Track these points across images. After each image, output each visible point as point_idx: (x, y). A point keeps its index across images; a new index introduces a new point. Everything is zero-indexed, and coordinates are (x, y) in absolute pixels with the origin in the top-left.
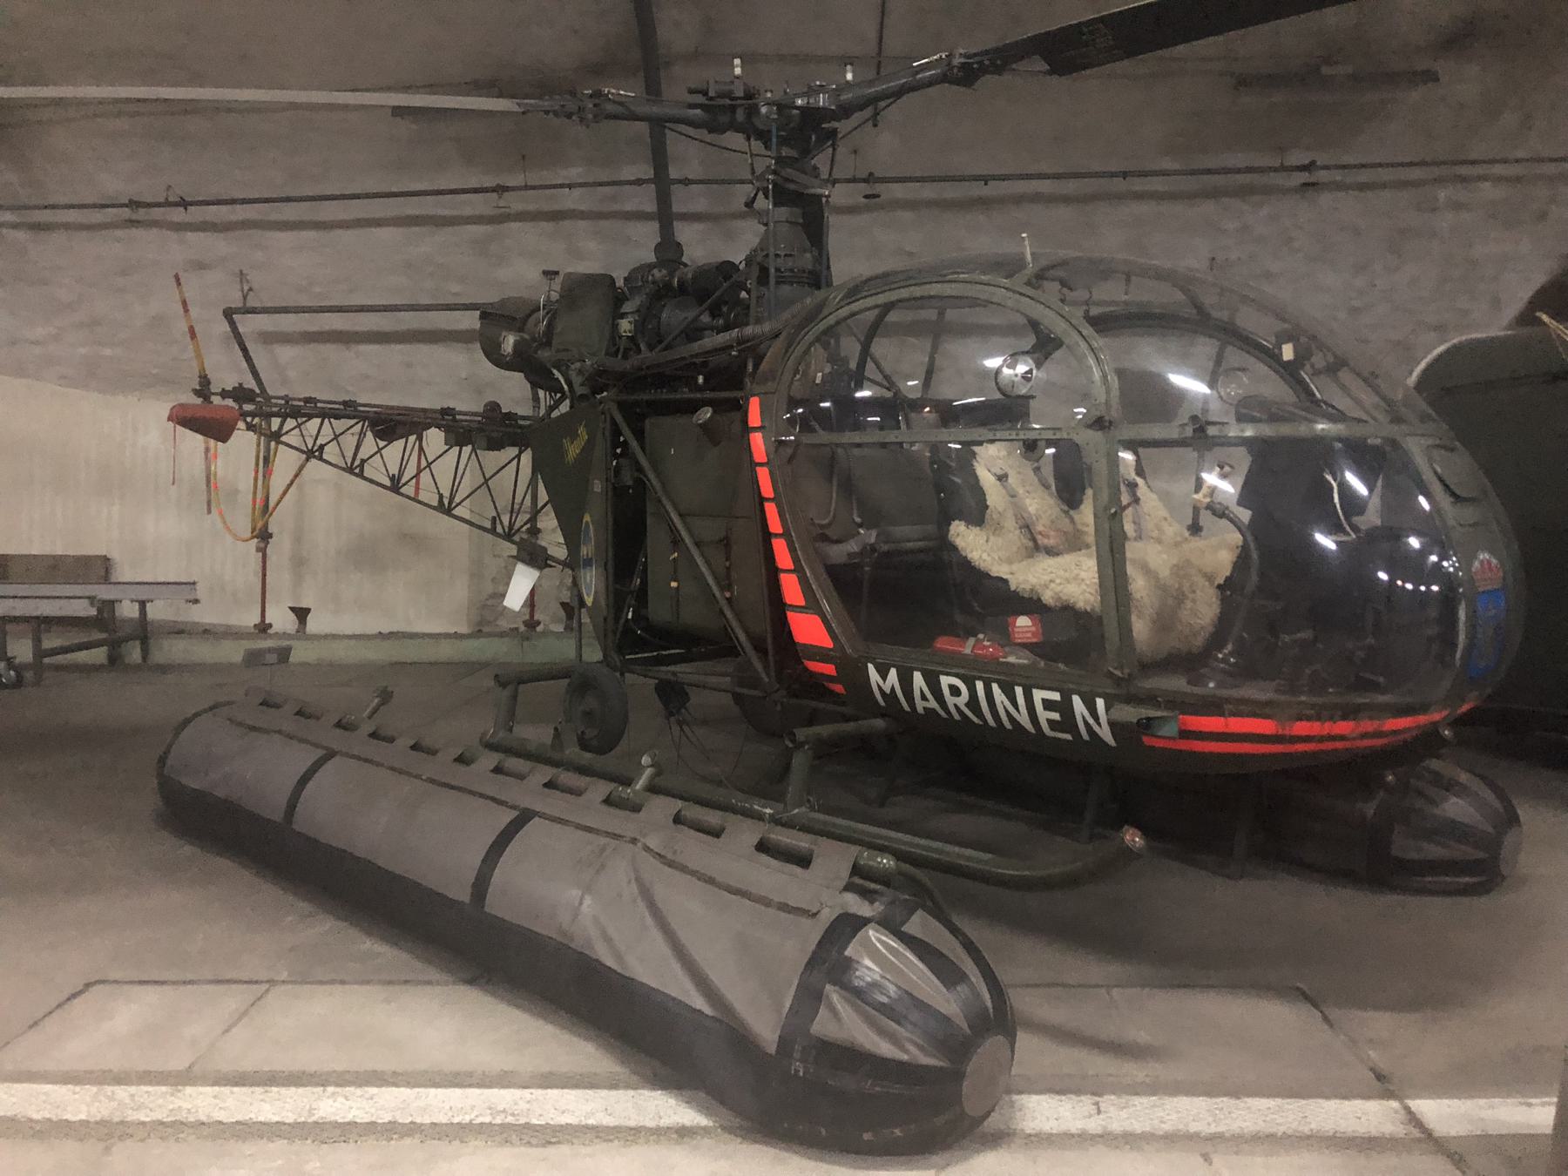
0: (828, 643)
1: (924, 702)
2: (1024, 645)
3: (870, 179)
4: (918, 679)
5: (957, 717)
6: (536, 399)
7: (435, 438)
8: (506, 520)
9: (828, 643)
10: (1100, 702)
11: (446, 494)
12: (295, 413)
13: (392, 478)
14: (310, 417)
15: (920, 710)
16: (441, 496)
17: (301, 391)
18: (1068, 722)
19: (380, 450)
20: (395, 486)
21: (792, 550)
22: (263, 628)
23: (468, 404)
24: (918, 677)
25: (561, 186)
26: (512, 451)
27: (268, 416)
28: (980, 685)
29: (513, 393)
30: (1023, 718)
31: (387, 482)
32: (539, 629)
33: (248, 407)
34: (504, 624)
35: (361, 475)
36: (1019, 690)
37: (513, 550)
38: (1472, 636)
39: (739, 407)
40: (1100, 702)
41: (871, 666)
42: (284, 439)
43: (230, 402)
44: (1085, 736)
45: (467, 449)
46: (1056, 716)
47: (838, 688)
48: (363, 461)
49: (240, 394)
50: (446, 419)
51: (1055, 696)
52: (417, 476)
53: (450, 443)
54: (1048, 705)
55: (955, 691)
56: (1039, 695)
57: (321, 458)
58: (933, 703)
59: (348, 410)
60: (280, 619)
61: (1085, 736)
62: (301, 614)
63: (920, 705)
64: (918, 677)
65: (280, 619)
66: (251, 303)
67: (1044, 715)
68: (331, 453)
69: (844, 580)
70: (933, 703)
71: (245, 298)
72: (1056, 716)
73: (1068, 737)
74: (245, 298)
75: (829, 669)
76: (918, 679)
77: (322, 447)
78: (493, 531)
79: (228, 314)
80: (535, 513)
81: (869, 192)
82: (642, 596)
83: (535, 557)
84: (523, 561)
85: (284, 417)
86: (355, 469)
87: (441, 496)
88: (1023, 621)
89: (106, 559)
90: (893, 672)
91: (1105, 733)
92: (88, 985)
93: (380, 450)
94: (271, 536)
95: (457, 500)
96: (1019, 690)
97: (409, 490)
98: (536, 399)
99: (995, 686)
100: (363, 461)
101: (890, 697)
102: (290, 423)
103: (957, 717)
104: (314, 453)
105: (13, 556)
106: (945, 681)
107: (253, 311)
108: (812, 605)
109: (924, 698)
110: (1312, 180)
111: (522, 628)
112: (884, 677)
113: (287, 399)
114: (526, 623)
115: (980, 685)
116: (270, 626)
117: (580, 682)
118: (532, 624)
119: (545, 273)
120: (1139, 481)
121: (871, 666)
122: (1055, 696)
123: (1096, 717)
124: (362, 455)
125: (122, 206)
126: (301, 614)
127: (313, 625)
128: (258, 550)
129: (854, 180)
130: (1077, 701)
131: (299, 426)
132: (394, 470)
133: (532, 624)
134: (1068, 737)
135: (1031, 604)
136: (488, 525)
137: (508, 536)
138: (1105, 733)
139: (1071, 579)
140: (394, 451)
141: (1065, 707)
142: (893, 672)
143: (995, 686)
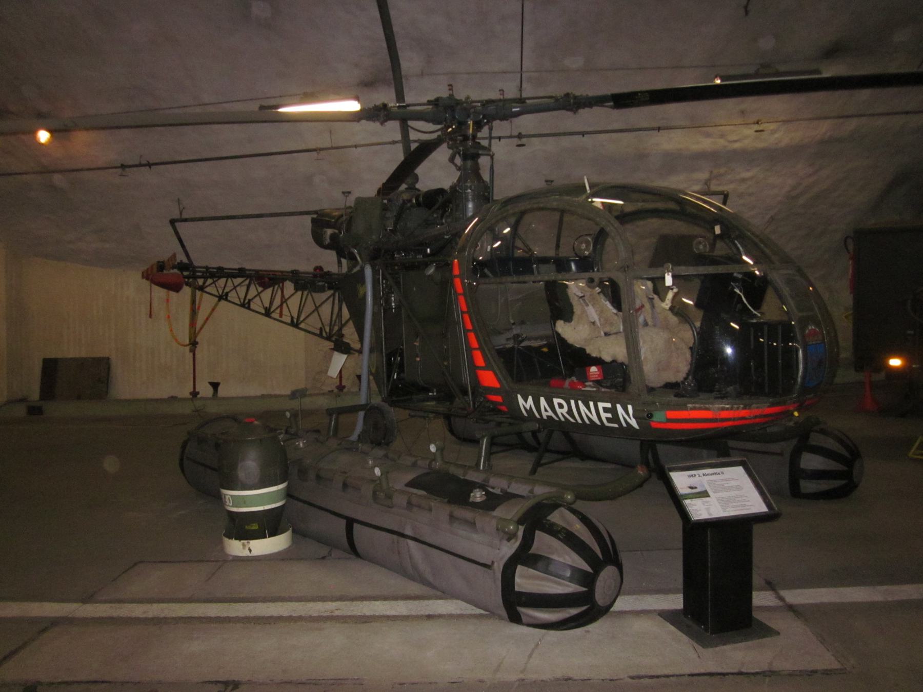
0: (498, 386)
1: (547, 413)
2: (593, 381)
3: (520, 136)
4: (543, 401)
5: (563, 419)
6: (340, 263)
7: (289, 287)
8: (327, 329)
9: (498, 386)
10: (630, 407)
11: (295, 316)
12: (212, 276)
13: (266, 309)
14: (219, 278)
15: (545, 417)
16: (292, 318)
17: (214, 264)
18: (615, 418)
19: (259, 294)
20: (268, 313)
21: (477, 337)
22: (195, 394)
23: (306, 267)
24: (542, 400)
25: (350, 147)
26: (331, 292)
27: (196, 278)
28: (572, 402)
29: (329, 261)
30: (595, 418)
31: (263, 311)
32: (345, 390)
33: (186, 273)
34: (327, 389)
35: (249, 308)
36: (591, 404)
37: (332, 345)
38: (805, 368)
39: (448, 266)
40: (630, 407)
41: (519, 396)
42: (207, 290)
43: (176, 271)
44: (624, 425)
45: (306, 293)
46: (609, 415)
47: (504, 408)
48: (250, 301)
49: (182, 267)
50: (296, 278)
51: (609, 405)
52: (281, 306)
53: (296, 289)
54: (606, 410)
55: (561, 406)
56: (601, 405)
57: (226, 299)
58: (550, 413)
59: (241, 273)
60: (205, 390)
61: (624, 425)
62: (215, 386)
63: (545, 414)
64: (542, 400)
65: (205, 390)
66: (185, 216)
67: (604, 416)
68: (232, 296)
69: (506, 355)
70: (550, 413)
71: (181, 214)
72: (609, 415)
73: (616, 426)
74: (181, 214)
75: (498, 399)
76: (543, 401)
77: (227, 294)
78: (320, 335)
79: (173, 222)
80: (342, 326)
81: (520, 143)
82: (401, 367)
83: (342, 347)
84: (337, 351)
85: (206, 278)
86: (246, 305)
87: (292, 318)
88: (594, 369)
89: (108, 359)
90: (530, 398)
91: (633, 422)
92: (135, 564)
93: (259, 294)
94: (197, 343)
95: (301, 319)
96: (591, 404)
97: (276, 315)
98: (340, 263)
99: (580, 402)
100: (250, 301)
101: (530, 411)
102: (210, 281)
103: (563, 419)
104: (223, 297)
105: (61, 359)
106: (556, 401)
107: (186, 220)
108: (488, 367)
109: (546, 410)
110: (761, 129)
111: (336, 391)
112: (526, 401)
113: (207, 268)
114: (338, 387)
115: (572, 402)
116: (198, 393)
117: (370, 410)
118: (341, 388)
119: (343, 193)
120: (656, 297)
121: (519, 396)
122: (609, 405)
123: (627, 416)
124: (249, 297)
125: (116, 168)
126: (215, 386)
127: (222, 392)
128: (191, 351)
129: (511, 137)
130: (619, 407)
131: (214, 282)
132: (267, 305)
133: (341, 388)
134: (616, 426)
135: (598, 362)
136: (318, 332)
137: (328, 338)
138: (633, 422)
139: (612, 350)
140: (267, 294)
141: (613, 411)
142: (530, 398)
143: (580, 402)
